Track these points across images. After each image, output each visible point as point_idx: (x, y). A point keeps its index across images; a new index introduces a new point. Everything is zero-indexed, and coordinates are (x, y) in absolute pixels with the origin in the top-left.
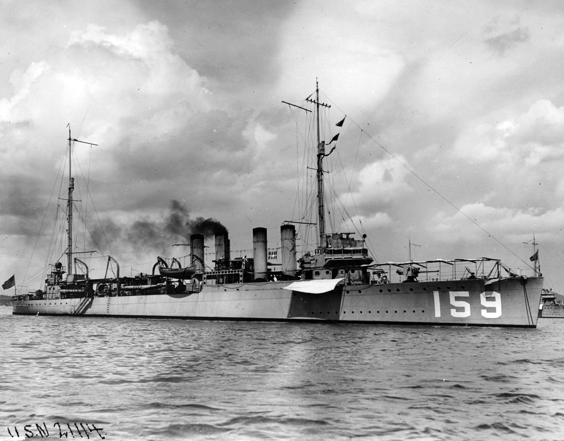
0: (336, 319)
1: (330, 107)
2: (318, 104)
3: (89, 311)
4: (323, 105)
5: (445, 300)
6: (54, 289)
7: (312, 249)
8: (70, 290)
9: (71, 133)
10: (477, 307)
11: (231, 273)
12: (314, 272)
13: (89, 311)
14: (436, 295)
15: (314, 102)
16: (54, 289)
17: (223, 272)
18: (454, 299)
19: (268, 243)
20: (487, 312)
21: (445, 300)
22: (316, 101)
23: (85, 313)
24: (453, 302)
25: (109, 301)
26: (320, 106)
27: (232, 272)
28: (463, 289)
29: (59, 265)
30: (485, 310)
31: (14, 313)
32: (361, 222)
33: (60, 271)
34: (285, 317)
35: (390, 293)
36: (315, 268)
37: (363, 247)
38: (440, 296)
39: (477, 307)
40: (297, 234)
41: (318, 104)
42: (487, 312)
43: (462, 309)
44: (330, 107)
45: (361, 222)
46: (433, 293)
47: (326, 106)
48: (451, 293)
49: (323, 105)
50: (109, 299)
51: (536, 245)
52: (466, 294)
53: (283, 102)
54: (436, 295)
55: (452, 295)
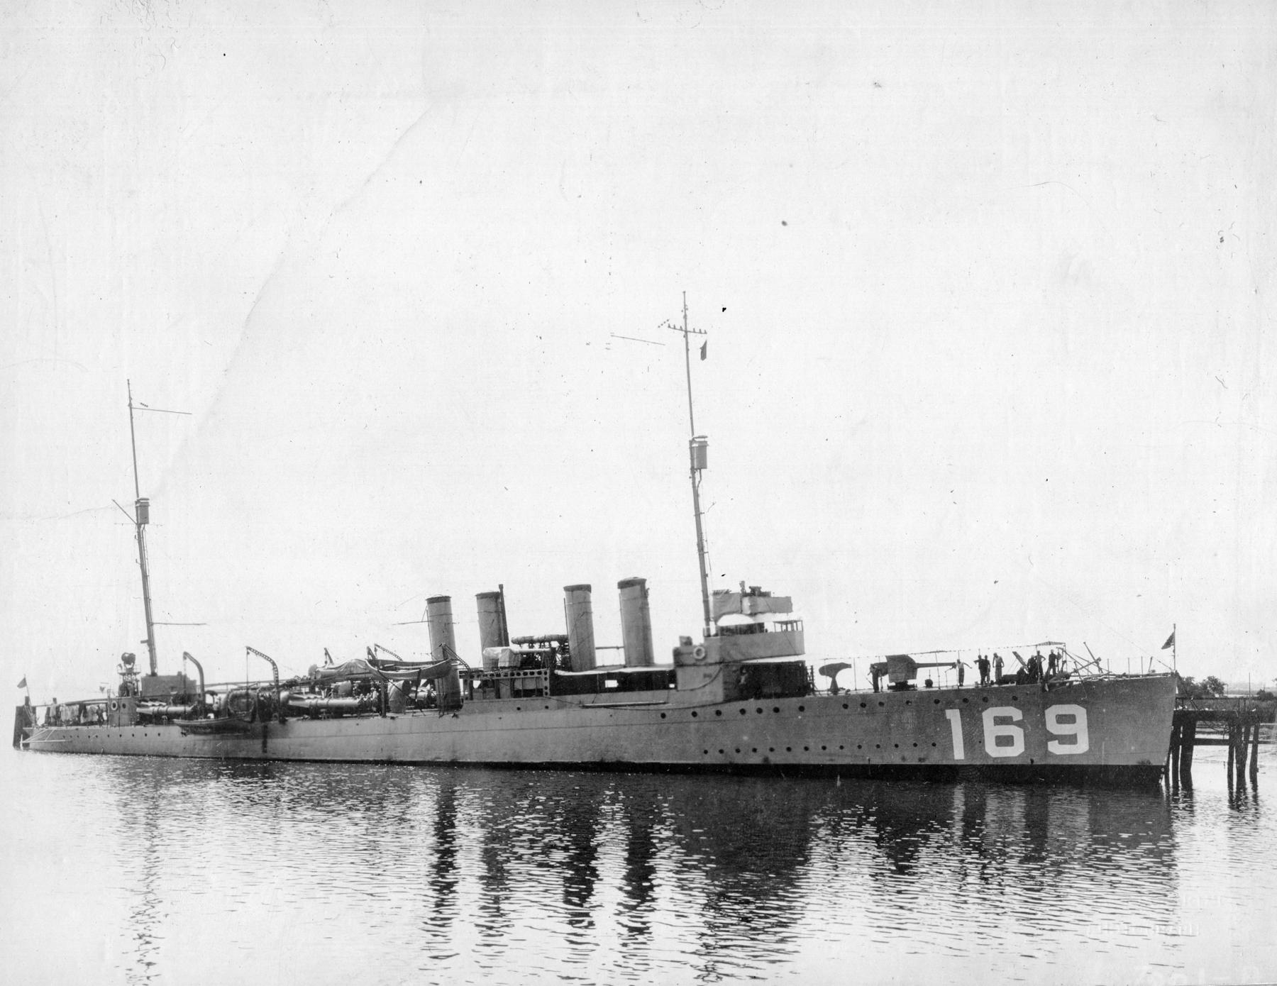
15: (681, 329)
22: (684, 328)
34: (431, 660)
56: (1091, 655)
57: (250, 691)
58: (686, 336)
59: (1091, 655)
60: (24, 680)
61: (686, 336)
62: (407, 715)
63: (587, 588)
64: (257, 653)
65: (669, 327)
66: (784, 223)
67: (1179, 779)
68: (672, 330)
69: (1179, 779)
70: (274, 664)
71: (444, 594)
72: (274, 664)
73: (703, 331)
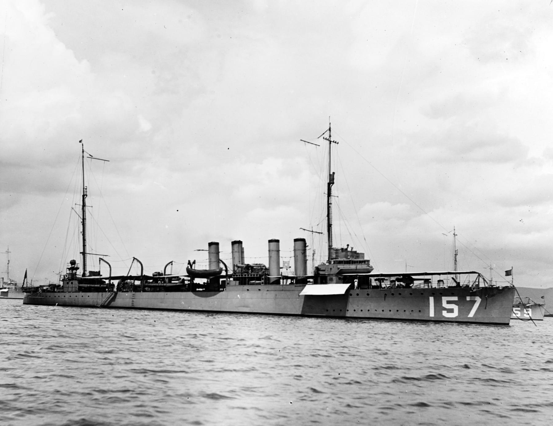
0: (344, 315)
1: (338, 143)
2: (330, 142)
3: (113, 304)
4: (334, 142)
5: (438, 302)
6: (72, 283)
7: (324, 259)
8: (91, 285)
9: (84, 146)
10: (523, 314)
11: (253, 276)
12: (328, 278)
13: (113, 304)
14: (432, 299)
15: (328, 140)
16: (72, 283)
17: (245, 275)
18: (446, 302)
19: (280, 252)
20: (447, 312)
21: (438, 302)
22: (329, 139)
23: (109, 305)
24: (445, 305)
25: (133, 296)
26: (332, 143)
27: (254, 275)
28: (453, 295)
29: (73, 262)
30: (446, 312)
31: (24, 303)
32: (365, 239)
33: (74, 267)
34: (300, 313)
35: (392, 296)
36: (329, 274)
37: (364, 259)
38: (532, 310)
39: (523, 314)
40: (308, 246)
41: (330, 142)
42: (447, 312)
43: (451, 311)
44: (338, 143)
45: (365, 239)
46: (441, 299)
47: (336, 142)
48: (443, 298)
49: (334, 142)
50: (134, 294)
51: (456, 236)
52: (455, 298)
53: (301, 140)
54: (432, 299)
55: (445, 299)
56: (131, 267)
57: (61, 279)
58: (330, 143)
59: (131, 267)
60: (81, 140)
61: (330, 143)
62: (220, 367)
63: (506, 275)
64: (138, 261)
65: (324, 138)
66: (228, 149)
67: (93, 285)
68: (325, 140)
69: (93, 285)
70: (110, 265)
71: (277, 239)
72: (110, 265)
73: (337, 142)
